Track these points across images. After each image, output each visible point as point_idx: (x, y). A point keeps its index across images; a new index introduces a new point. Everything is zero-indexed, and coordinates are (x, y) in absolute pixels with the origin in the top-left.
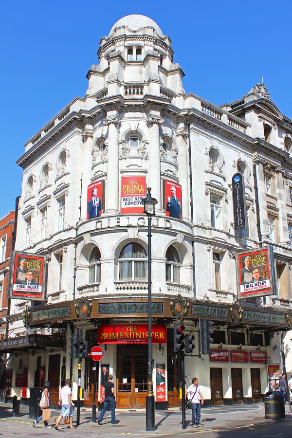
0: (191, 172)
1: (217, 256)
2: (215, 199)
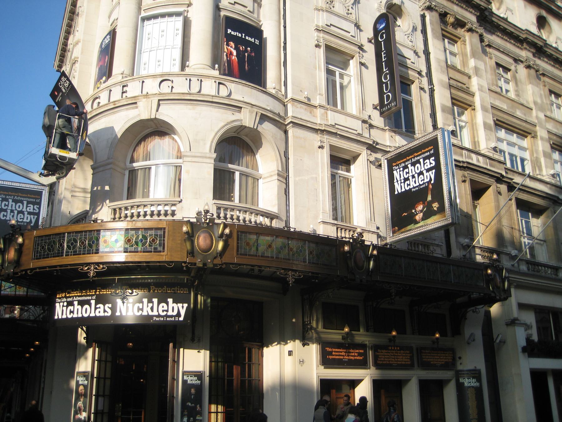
0: (285, 10)
1: (340, 161)
2: (336, 57)
